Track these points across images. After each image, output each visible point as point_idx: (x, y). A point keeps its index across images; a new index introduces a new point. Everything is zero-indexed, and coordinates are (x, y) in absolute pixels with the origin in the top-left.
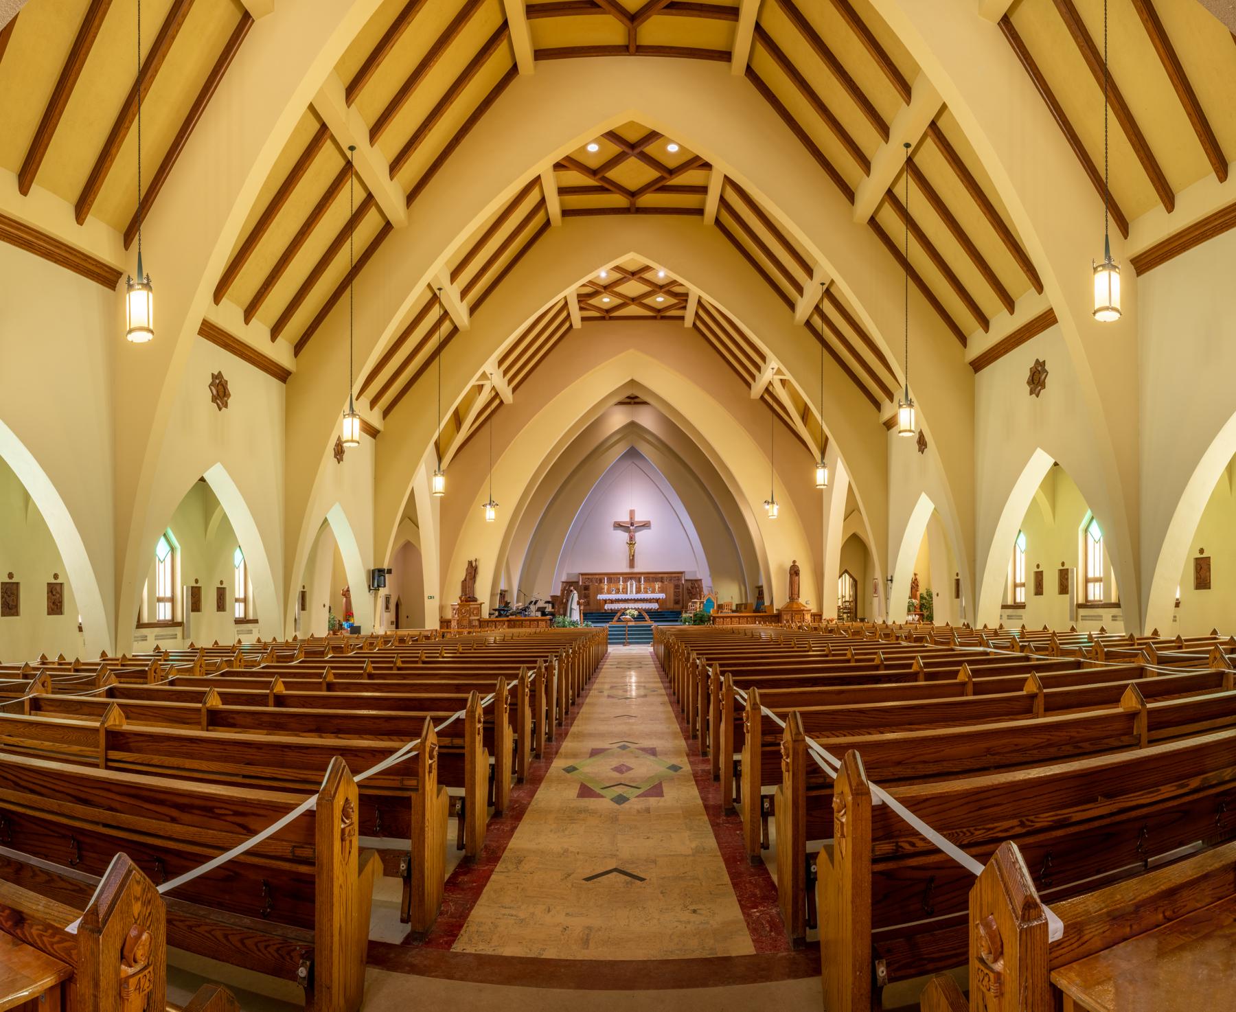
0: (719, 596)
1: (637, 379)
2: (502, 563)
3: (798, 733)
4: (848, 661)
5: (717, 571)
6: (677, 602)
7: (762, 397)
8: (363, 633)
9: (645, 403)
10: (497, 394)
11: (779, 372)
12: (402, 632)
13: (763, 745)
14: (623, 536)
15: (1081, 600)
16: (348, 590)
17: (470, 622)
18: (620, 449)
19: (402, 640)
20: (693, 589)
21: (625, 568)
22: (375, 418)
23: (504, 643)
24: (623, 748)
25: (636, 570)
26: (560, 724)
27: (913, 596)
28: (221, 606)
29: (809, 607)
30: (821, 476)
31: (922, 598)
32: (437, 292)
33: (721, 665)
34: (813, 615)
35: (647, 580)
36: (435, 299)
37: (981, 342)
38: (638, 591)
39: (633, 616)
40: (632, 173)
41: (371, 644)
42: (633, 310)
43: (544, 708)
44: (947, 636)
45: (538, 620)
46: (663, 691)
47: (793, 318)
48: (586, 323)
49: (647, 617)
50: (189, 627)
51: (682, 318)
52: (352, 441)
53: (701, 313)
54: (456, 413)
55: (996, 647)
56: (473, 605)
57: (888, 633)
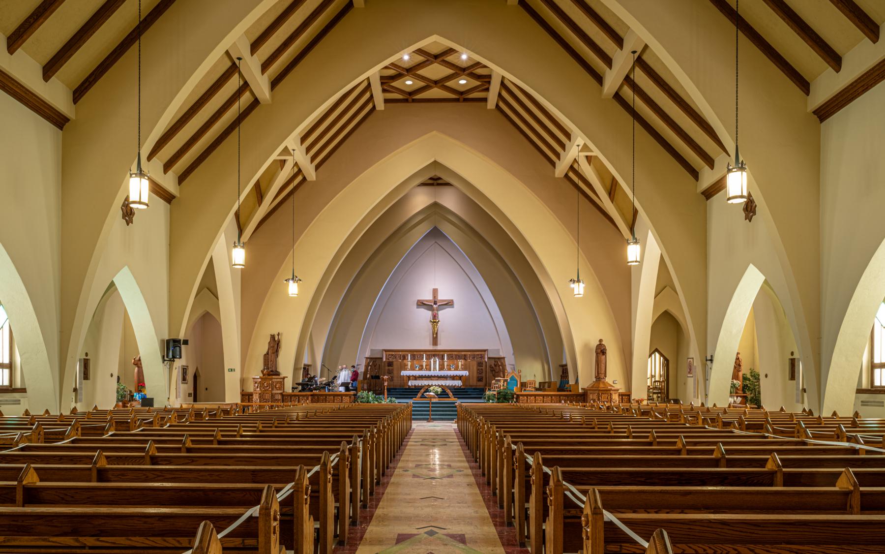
0: (522, 374)
1: (440, 160)
3: (558, 480)
4: (678, 452)
5: (520, 348)
6: (480, 379)
7: (566, 176)
8: (156, 405)
9: (448, 184)
10: (300, 171)
11: (585, 148)
12: (199, 405)
13: (565, 517)
14: (427, 314)
16: (140, 360)
17: (273, 395)
18: (423, 230)
19: (198, 414)
20: (496, 367)
21: (427, 345)
22: (169, 182)
23: (308, 420)
24: (431, 533)
25: (439, 347)
26: (364, 506)
27: (735, 376)
29: (616, 387)
30: (633, 252)
31: (745, 379)
32: (237, 62)
33: (512, 437)
35: (450, 357)
36: (234, 68)
37: (828, 84)
38: (442, 368)
39: (436, 393)
41: (163, 418)
42: (436, 92)
43: (348, 490)
44: (788, 425)
45: (342, 395)
46: (469, 472)
47: (601, 91)
48: (388, 105)
49: (451, 394)
51: (485, 100)
52: (140, 203)
53: (505, 94)
54: (257, 185)
55: (867, 443)
56: (275, 379)
57: (712, 416)
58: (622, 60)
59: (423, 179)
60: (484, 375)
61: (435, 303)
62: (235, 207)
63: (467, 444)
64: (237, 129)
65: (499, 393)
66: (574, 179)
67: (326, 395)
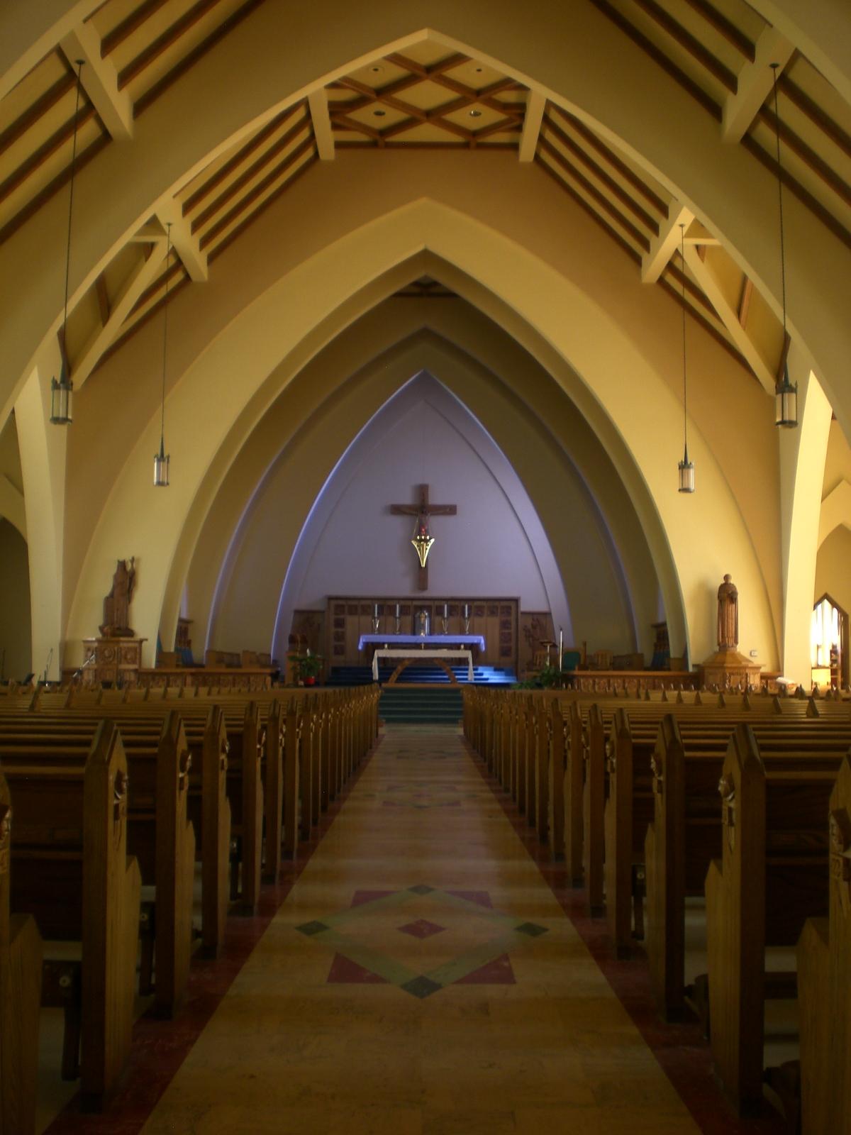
7: (661, 281)
10: (179, 264)
17: (120, 673)
25: (426, 594)
32: (76, 67)
36: (71, 79)
42: (426, 132)
51: (515, 147)
53: (551, 137)
54: (101, 284)
56: (125, 643)
58: (754, 83)
60: (513, 644)
62: (59, 322)
64: (70, 183)
66: (677, 288)
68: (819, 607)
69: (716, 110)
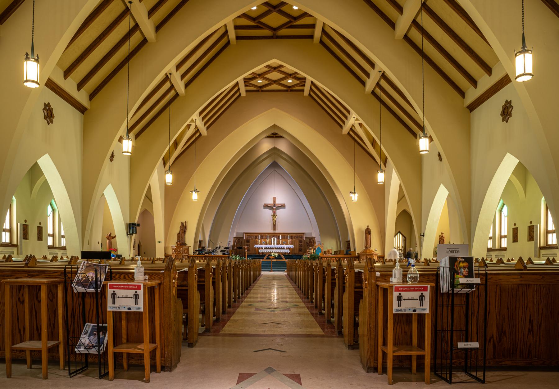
2: (200, 227)
5: (323, 232)
6: (300, 250)
7: (349, 133)
9: (281, 137)
10: (198, 130)
11: (357, 120)
14: (269, 212)
15: (542, 244)
18: (267, 163)
20: (310, 242)
25: (277, 232)
28: (40, 238)
29: (376, 252)
30: (381, 177)
34: (379, 257)
37: (473, 94)
38: (278, 243)
40: (274, 20)
42: (275, 87)
47: (364, 90)
48: (248, 93)
49: (283, 257)
50: (21, 248)
51: (303, 91)
53: (313, 88)
58: (374, 77)
59: (269, 134)
61: (274, 206)
63: (292, 279)
65: (311, 256)
67: (212, 257)
68: (396, 236)
69: (364, 83)
